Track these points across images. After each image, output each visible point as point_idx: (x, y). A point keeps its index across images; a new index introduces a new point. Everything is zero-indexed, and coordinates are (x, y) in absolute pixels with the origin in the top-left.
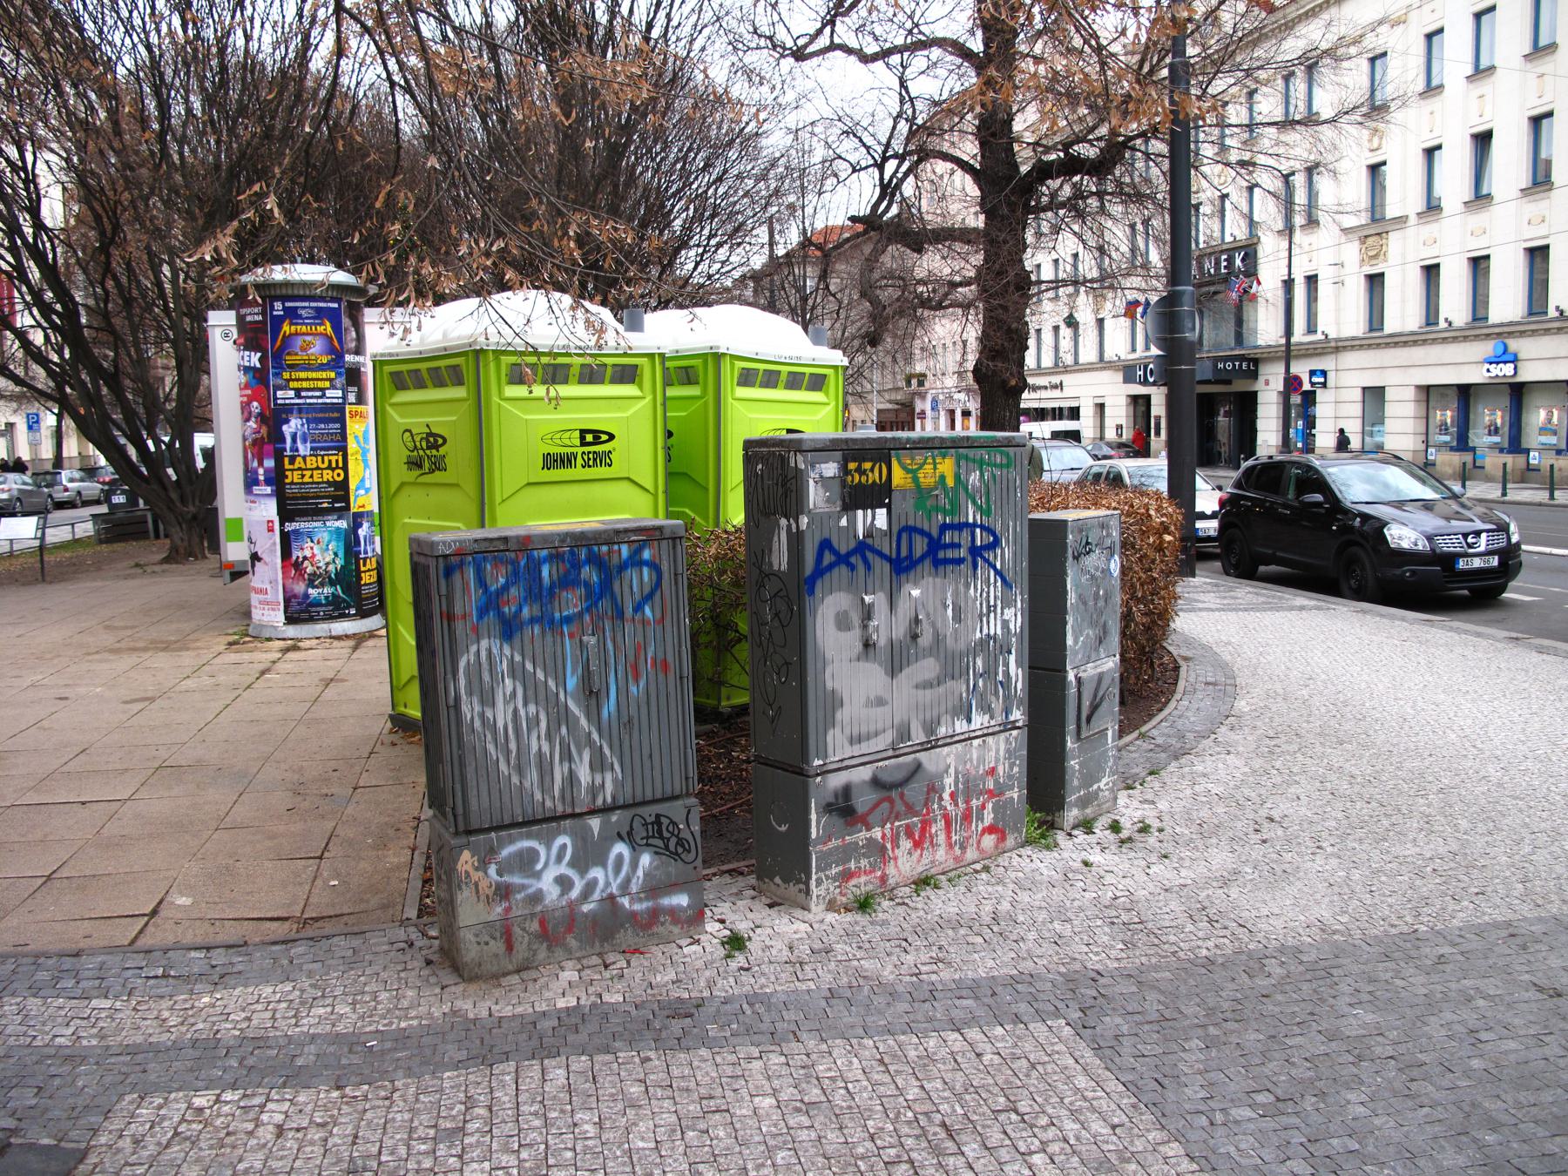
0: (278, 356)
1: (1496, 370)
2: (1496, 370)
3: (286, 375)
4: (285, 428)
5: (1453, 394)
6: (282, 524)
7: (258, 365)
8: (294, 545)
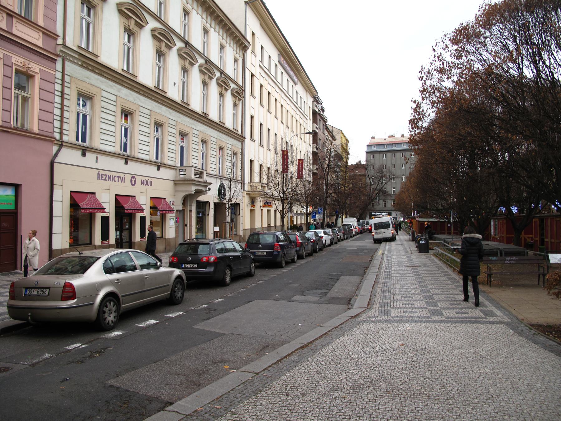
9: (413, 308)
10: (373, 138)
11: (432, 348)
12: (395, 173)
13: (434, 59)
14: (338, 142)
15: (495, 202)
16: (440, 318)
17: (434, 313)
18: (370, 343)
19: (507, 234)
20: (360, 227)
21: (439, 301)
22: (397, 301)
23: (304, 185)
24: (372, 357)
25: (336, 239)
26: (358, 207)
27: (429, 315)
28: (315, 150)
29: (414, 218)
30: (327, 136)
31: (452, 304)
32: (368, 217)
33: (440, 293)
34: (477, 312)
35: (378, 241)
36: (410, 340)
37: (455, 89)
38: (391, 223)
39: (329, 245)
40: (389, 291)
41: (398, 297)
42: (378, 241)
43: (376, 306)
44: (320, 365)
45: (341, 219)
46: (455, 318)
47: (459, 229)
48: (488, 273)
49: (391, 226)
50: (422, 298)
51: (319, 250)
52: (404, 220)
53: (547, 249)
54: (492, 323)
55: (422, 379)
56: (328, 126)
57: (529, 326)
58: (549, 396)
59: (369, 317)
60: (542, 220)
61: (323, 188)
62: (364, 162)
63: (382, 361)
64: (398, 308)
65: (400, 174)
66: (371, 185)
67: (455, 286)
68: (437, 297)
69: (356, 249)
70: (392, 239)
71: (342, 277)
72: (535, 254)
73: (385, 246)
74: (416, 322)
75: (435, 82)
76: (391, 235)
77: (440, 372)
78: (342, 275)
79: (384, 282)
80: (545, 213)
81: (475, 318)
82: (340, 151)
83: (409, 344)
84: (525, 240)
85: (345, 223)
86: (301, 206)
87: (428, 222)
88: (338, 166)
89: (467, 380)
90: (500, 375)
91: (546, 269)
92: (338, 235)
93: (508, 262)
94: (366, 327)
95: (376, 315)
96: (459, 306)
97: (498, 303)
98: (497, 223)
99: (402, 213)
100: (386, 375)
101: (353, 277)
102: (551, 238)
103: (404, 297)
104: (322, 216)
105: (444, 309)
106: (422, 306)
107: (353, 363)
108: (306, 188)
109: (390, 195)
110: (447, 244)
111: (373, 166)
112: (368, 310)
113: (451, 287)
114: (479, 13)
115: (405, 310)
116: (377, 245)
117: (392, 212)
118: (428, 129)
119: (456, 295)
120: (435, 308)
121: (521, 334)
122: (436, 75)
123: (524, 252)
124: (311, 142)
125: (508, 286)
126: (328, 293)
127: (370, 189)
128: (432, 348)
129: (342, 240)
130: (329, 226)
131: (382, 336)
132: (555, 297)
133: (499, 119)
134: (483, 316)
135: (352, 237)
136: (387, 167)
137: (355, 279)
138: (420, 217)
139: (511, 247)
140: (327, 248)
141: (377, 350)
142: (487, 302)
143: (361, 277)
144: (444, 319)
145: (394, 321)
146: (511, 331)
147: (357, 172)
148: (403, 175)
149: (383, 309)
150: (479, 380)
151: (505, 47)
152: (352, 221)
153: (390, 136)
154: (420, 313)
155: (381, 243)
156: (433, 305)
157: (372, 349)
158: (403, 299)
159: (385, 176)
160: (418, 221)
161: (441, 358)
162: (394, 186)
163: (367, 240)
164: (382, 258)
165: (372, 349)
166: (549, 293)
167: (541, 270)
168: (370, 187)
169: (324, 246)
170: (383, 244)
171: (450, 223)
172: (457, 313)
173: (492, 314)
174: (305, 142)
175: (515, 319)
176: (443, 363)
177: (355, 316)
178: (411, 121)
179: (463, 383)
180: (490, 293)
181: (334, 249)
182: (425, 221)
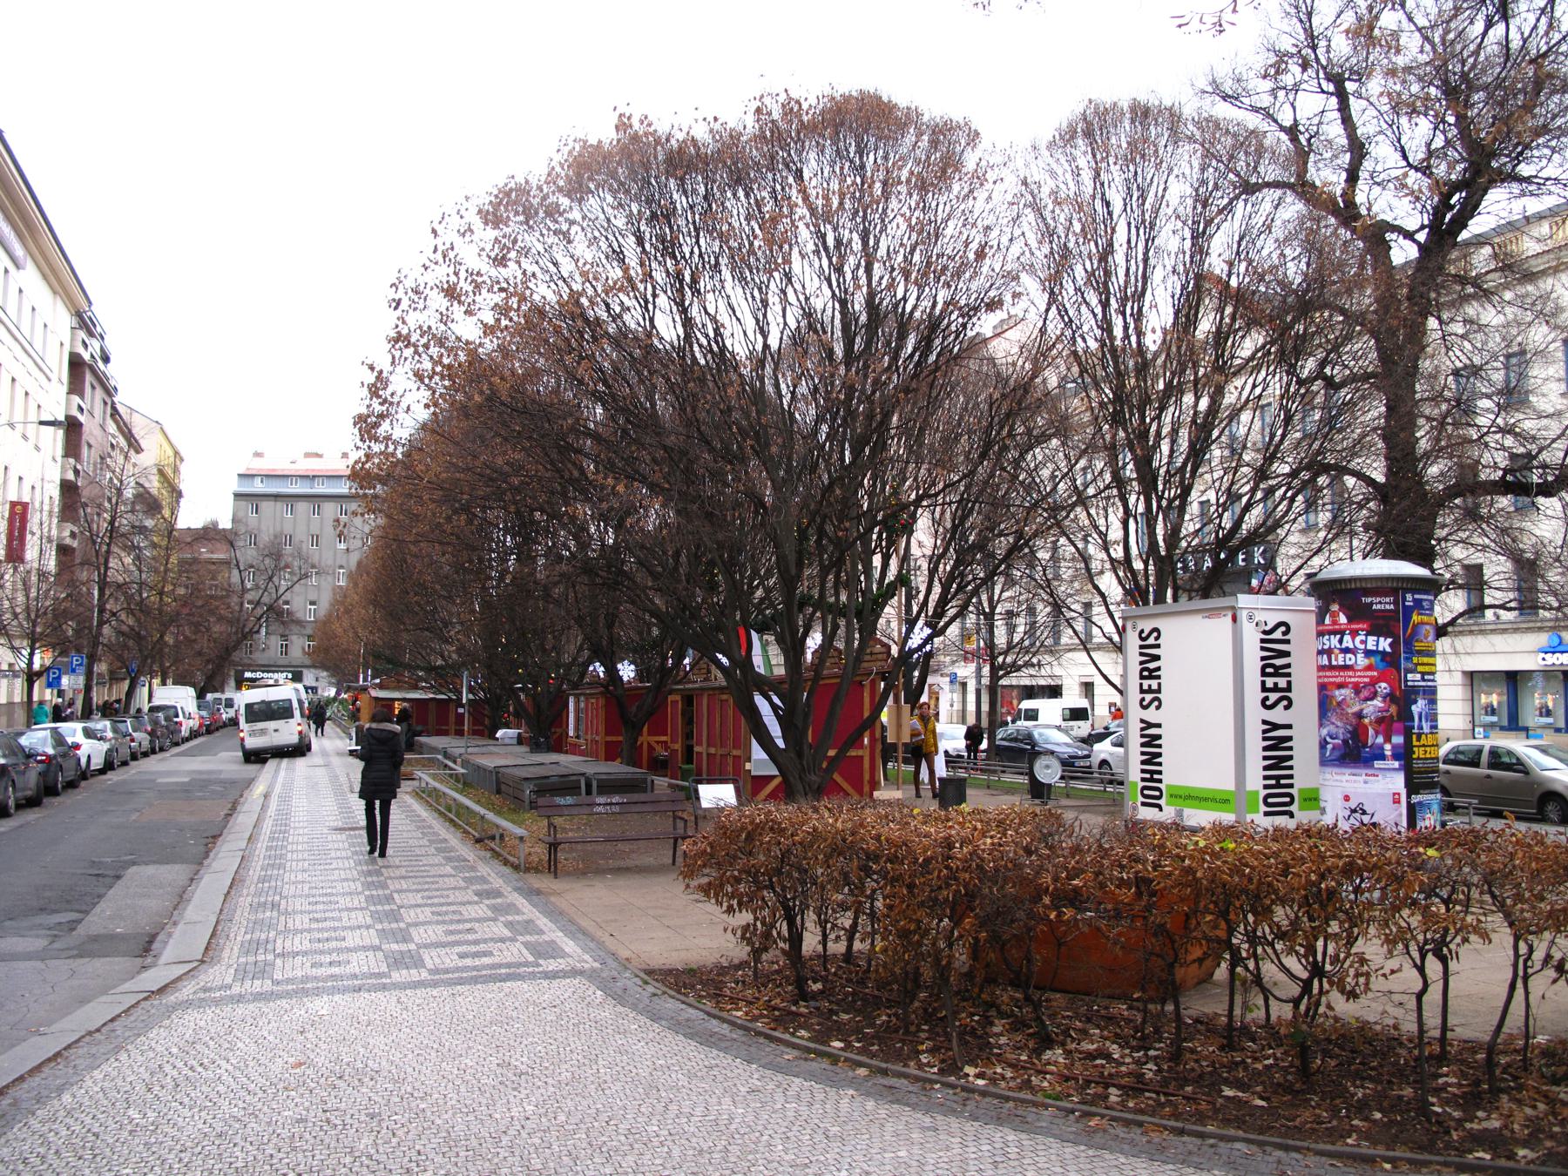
0: (1409, 643)
1: (1551, 659)
2: (1551, 659)
3: (1415, 660)
4: (1413, 708)
5: (1561, 676)
6: (1409, 796)
7: (1388, 649)
8: (1419, 816)
9: (339, 950)
10: (258, 455)
11: (384, 1063)
12: (316, 560)
13: (432, 256)
14: (147, 459)
15: (581, 649)
16: (415, 975)
17: (398, 961)
18: (200, 1069)
20: (204, 713)
21: (416, 925)
22: (296, 932)
23: (24, 584)
24: (203, 1114)
25: (125, 753)
26: (200, 653)
27: (384, 968)
28: (71, 476)
29: (365, 689)
30: (114, 436)
31: (452, 933)
32: (232, 683)
33: (420, 901)
34: (515, 951)
35: (256, 757)
36: (324, 1046)
37: (481, 345)
38: (295, 705)
39: (102, 771)
40: (275, 906)
41: (300, 921)
42: (256, 757)
43: (231, 954)
44: (21, 1167)
45: (146, 690)
46: (458, 969)
47: (487, 722)
48: (551, 840)
49: (297, 713)
50: (369, 920)
51: (64, 788)
52: (338, 693)
53: (699, 773)
54: (551, 976)
55: (348, 1160)
56: (119, 407)
57: (642, 975)
58: (676, 1152)
59: (205, 990)
60: (689, 699)
61: (90, 594)
62: (225, 523)
63: (231, 1122)
64: (297, 954)
65: (330, 562)
66: (244, 590)
67: (464, 879)
68: (409, 916)
69: (186, 780)
70: (300, 750)
71: (133, 869)
72: (671, 786)
73: (277, 771)
74: (344, 990)
75: (430, 319)
76: (295, 739)
77: (400, 1133)
78: (134, 863)
79: (262, 880)
80: (697, 682)
81: (509, 965)
82: (154, 485)
83: (320, 1061)
84: (651, 748)
85: (156, 702)
86: (13, 648)
87: (404, 700)
88: (142, 530)
89: (474, 1143)
90: (561, 1118)
91: (691, 824)
92: (133, 740)
93: (600, 809)
94: (190, 1022)
95: (229, 980)
96: (470, 937)
97: (572, 922)
98: (582, 705)
99: (332, 676)
100: (240, 1164)
101: (168, 867)
102: (709, 745)
103: (317, 920)
104: (81, 681)
105: (426, 946)
106: (367, 942)
107: (137, 1140)
108: (33, 594)
109: (300, 623)
110: (450, 764)
111: (254, 538)
112: (204, 966)
113: (451, 882)
114: (558, 158)
115: (318, 958)
116: (253, 768)
117: (305, 671)
118: (413, 448)
119: (464, 904)
120: (404, 947)
121: (620, 998)
122: (438, 301)
123: (645, 781)
124: (59, 451)
125: (600, 872)
126: (79, 921)
127: (242, 604)
128: (384, 1063)
129: (145, 755)
130: (108, 710)
131: (240, 1045)
132: (700, 896)
133: (596, 436)
134: (531, 959)
135: (177, 744)
136: (296, 540)
137: (173, 873)
138: (381, 687)
139: (616, 768)
140: (91, 781)
141: (221, 1088)
142: (545, 920)
143: (194, 867)
144: (425, 975)
145: (280, 996)
146: (599, 993)
147: (204, 552)
148: (341, 567)
149: (251, 959)
150: (505, 1140)
151: (619, 256)
152: (181, 698)
153: (308, 455)
154: (359, 963)
155: (264, 761)
156: (399, 937)
157: (204, 1088)
158: (314, 925)
159: (287, 566)
160: (377, 699)
161: (409, 1089)
162: (313, 597)
163: (224, 755)
164: (264, 808)
165: (204, 1088)
166: (688, 886)
167: (680, 824)
168: (241, 597)
169: (85, 774)
170: (272, 764)
171: (462, 706)
172: (462, 956)
173: (552, 951)
174: (37, 448)
175: (610, 961)
176: (413, 1105)
177: (162, 990)
178: (360, 420)
179: (462, 1154)
180: (555, 893)
181: (117, 784)
182: (394, 700)
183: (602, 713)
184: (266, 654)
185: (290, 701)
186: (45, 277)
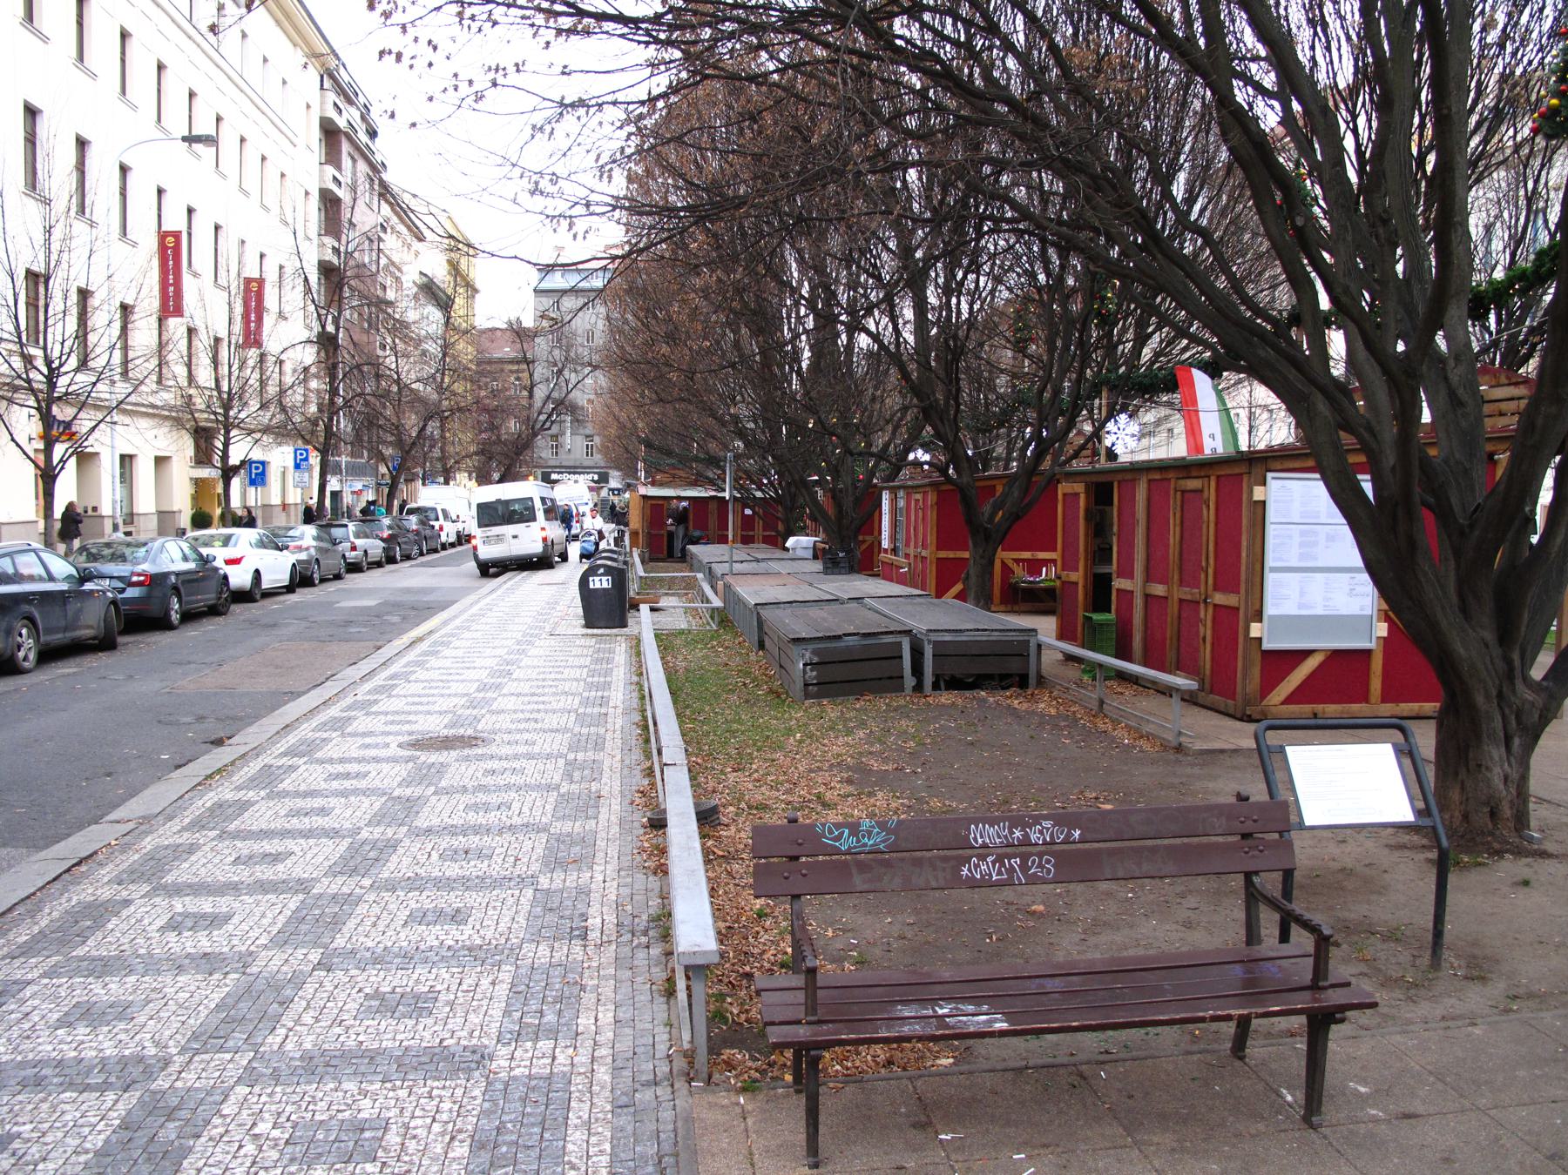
19: (939, 548)
28: (329, 256)
38: (538, 505)
49: (540, 515)
76: (537, 548)
98: (901, 503)
102: (1149, 578)
129: (379, 565)
135: (436, 551)
160: (644, 497)
183: (932, 516)
184: (572, 456)
185: (531, 499)
186: (278, 22)
